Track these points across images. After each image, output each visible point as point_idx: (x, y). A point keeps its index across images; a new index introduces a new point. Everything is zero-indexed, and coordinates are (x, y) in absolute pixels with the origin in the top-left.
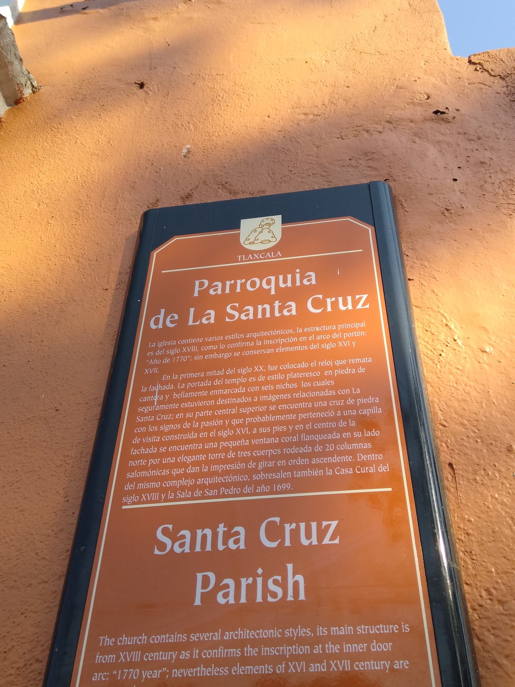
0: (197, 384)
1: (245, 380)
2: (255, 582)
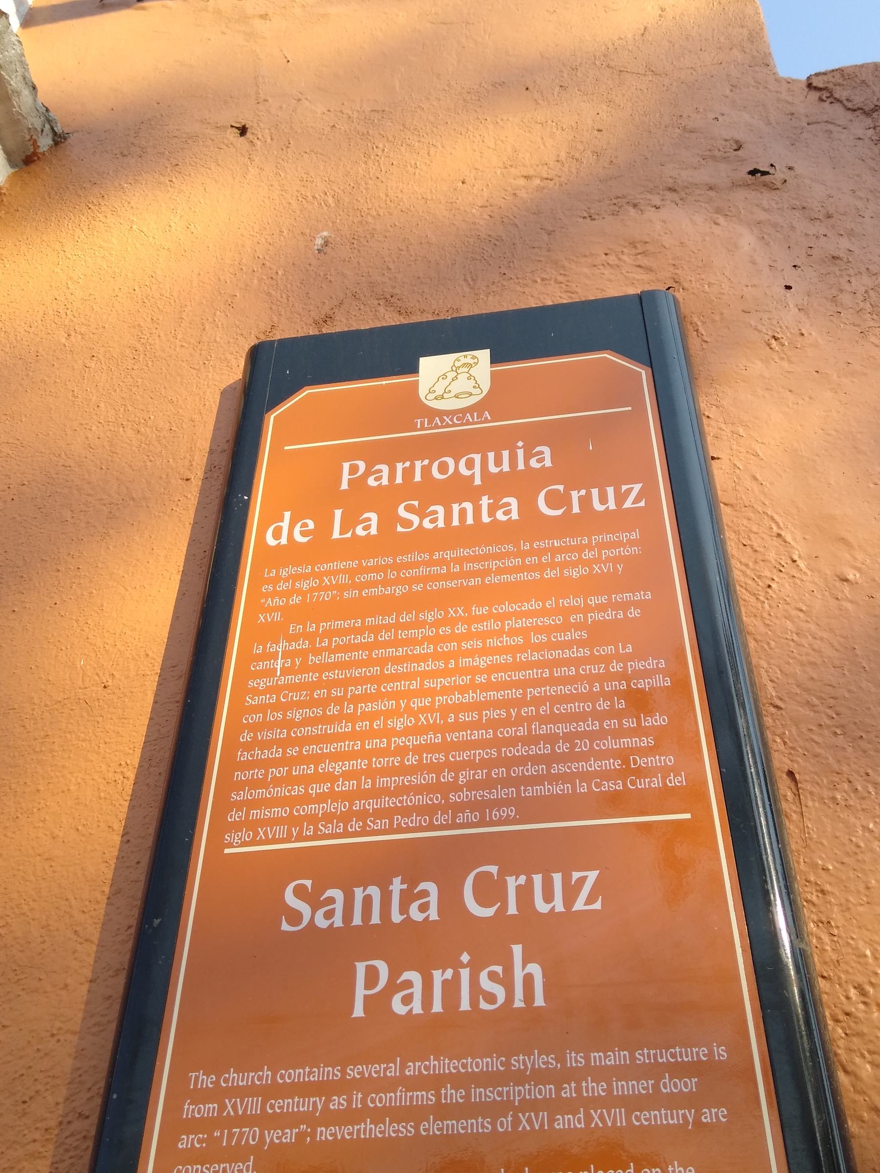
0: (350, 639)
2: (457, 976)
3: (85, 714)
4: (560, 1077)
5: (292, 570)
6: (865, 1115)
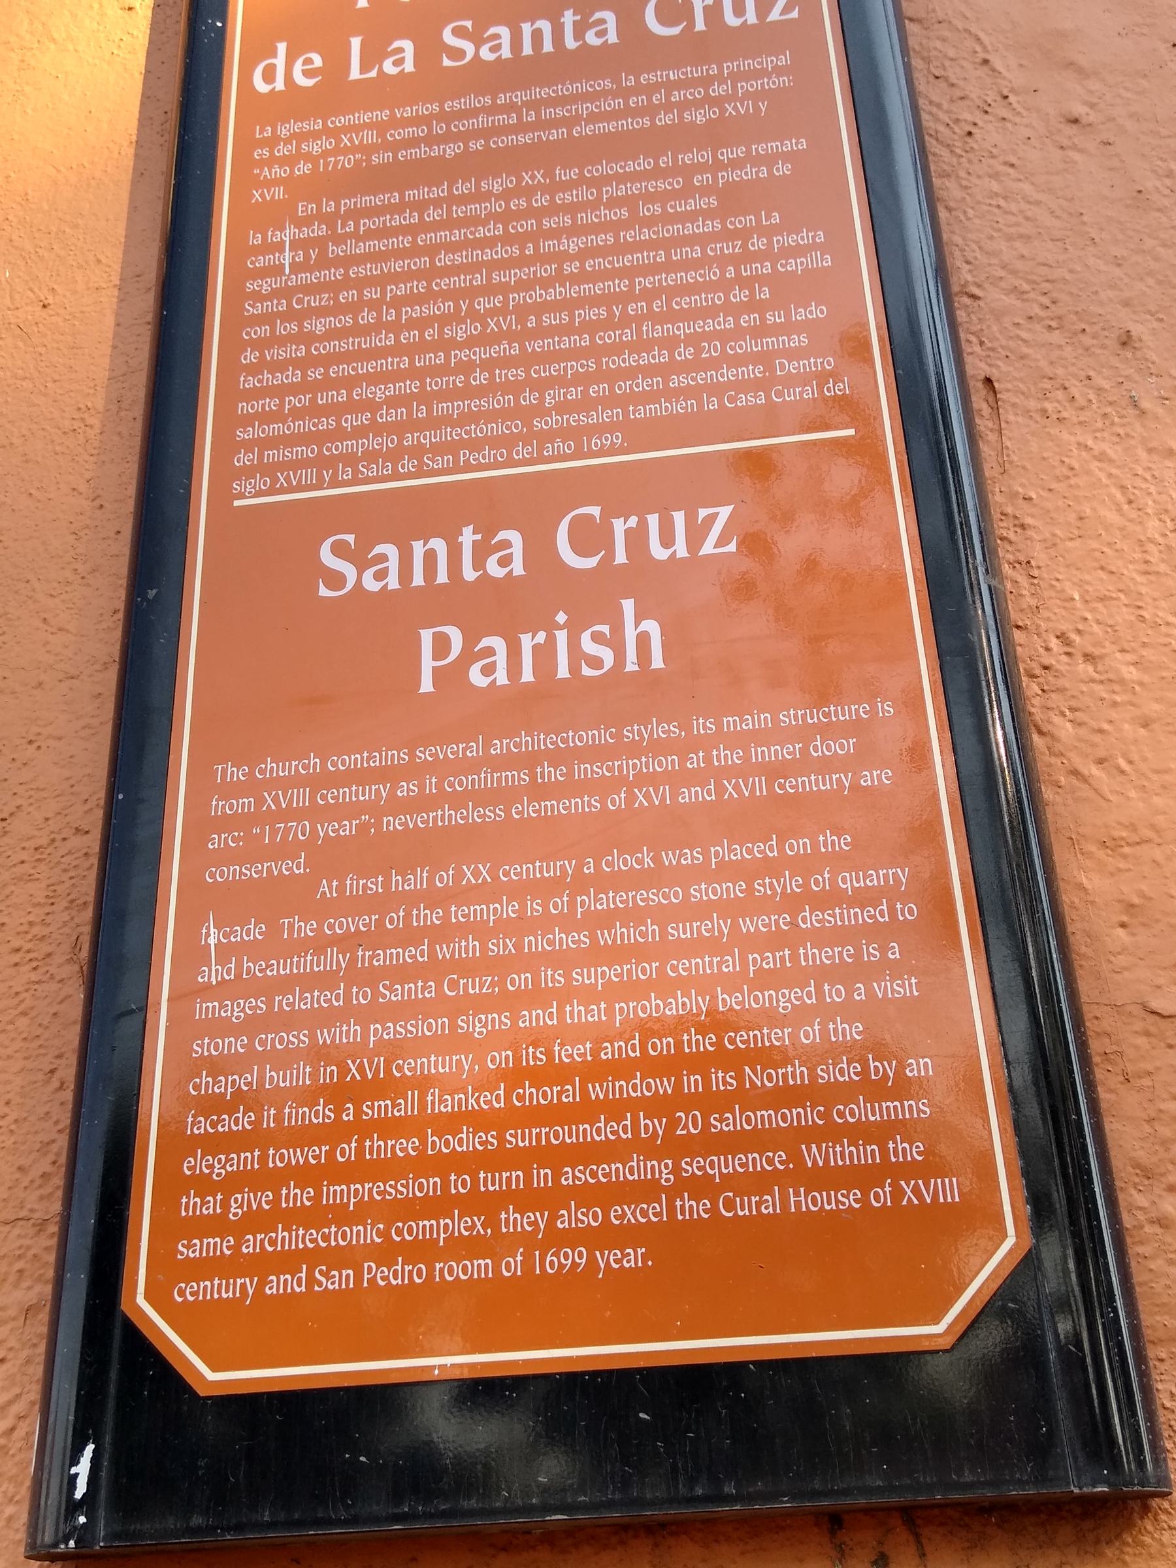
0: (384, 221)
1: (500, 206)
2: (551, 640)
3: (21, 344)
4: (684, 748)
5: (296, 127)
6: (1062, 779)
